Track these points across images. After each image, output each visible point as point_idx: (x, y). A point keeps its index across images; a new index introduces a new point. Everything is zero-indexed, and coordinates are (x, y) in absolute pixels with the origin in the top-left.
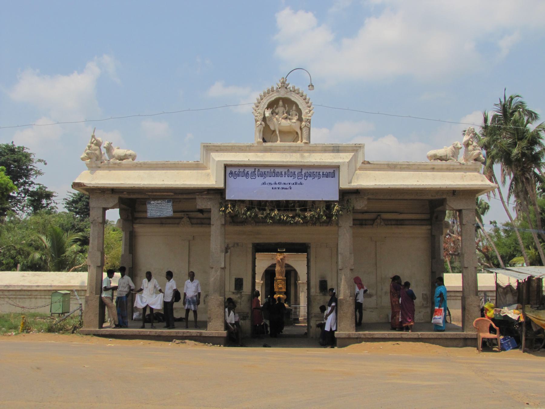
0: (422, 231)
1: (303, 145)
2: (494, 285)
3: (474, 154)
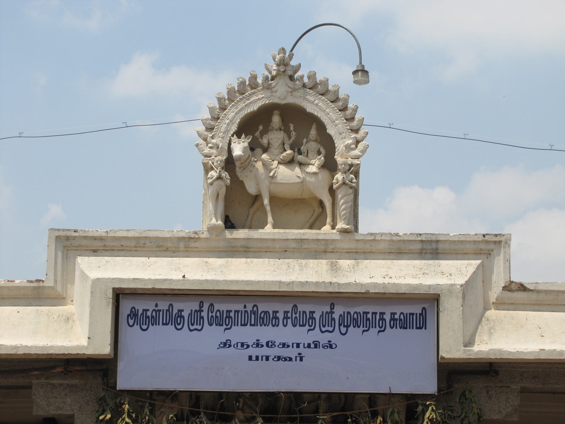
1: (338, 237)
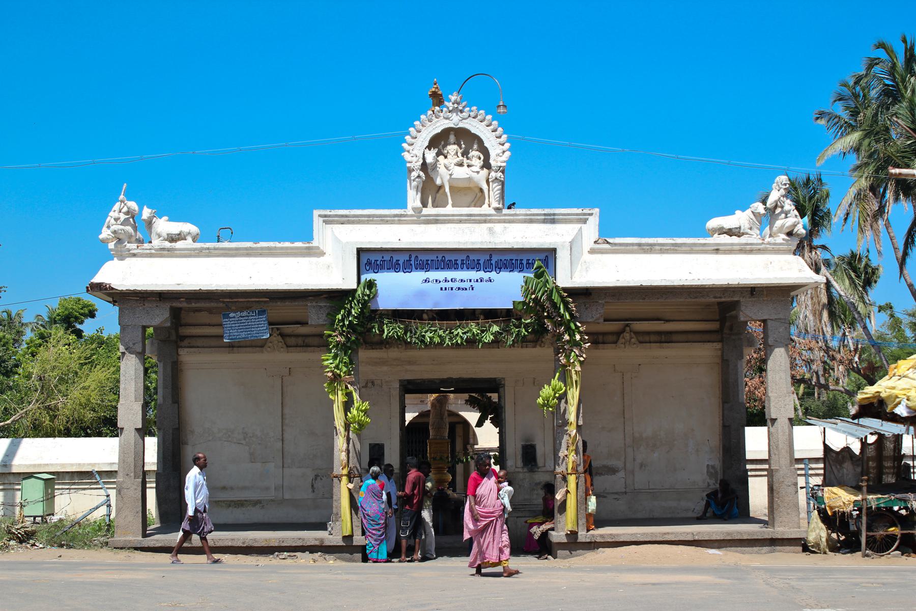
0: (707, 352)
1: (493, 212)
2: (822, 447)
3: (787, 225)
